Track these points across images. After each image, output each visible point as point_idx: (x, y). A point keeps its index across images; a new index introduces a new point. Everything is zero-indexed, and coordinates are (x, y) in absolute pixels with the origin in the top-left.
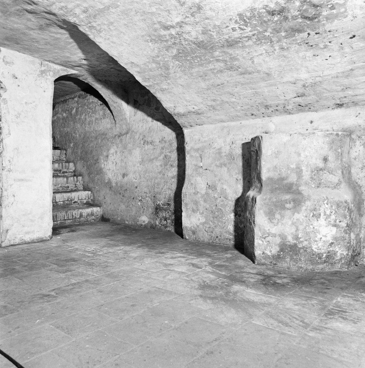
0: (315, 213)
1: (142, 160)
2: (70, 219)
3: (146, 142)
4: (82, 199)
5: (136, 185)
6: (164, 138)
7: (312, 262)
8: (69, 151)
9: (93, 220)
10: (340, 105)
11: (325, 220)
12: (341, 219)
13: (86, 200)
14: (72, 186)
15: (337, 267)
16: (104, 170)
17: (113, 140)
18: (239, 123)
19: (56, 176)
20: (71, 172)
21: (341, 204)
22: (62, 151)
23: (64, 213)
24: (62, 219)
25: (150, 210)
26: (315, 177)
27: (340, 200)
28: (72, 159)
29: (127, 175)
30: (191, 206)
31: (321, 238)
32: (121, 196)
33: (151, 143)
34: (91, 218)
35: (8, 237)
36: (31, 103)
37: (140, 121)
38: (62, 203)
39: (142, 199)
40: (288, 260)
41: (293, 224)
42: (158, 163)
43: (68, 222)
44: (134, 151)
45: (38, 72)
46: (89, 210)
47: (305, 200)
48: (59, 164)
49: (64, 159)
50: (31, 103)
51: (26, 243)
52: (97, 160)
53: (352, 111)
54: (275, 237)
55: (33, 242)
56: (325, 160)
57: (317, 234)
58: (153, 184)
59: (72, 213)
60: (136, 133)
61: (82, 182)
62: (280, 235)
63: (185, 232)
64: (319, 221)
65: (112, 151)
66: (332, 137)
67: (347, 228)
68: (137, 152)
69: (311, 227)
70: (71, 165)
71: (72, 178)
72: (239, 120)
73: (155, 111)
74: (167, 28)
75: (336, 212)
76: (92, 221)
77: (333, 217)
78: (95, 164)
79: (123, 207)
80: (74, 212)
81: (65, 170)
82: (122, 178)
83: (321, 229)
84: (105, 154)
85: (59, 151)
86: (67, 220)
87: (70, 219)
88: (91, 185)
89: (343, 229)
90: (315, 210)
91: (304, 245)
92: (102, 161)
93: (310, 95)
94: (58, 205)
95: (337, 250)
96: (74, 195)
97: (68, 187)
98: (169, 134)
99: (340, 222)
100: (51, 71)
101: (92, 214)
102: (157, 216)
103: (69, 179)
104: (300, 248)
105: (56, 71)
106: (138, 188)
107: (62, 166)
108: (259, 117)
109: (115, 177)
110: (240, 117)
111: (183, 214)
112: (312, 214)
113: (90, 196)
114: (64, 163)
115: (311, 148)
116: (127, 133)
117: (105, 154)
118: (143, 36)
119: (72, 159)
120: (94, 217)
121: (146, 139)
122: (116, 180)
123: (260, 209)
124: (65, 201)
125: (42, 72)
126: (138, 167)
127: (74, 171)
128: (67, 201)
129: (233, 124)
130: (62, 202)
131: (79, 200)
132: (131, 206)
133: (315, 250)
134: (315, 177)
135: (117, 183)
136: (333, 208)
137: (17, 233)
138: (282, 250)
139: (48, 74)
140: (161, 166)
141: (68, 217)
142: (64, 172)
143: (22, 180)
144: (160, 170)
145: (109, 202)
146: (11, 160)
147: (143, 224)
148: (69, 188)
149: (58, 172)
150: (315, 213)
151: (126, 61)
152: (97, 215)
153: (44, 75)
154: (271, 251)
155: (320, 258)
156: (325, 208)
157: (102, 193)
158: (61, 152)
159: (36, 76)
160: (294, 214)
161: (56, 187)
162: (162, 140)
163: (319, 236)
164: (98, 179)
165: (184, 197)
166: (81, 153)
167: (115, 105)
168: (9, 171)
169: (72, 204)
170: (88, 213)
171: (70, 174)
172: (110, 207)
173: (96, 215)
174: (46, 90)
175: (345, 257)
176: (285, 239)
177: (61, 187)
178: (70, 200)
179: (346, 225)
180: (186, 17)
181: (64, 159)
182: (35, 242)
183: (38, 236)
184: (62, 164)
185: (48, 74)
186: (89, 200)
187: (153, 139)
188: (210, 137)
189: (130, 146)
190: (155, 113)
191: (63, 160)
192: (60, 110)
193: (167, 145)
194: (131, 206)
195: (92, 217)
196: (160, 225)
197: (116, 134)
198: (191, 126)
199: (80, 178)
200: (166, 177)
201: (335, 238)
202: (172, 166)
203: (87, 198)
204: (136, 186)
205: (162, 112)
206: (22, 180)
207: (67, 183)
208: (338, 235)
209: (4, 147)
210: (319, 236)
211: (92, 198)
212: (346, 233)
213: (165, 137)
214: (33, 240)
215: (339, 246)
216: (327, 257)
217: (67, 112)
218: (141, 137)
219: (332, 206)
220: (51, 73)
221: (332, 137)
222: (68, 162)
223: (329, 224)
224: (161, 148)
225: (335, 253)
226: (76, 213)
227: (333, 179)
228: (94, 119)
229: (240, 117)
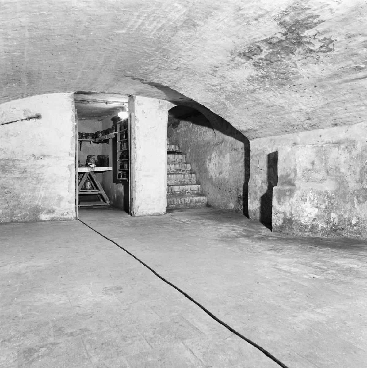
0: (303, 198)
1: (231, 162)
3: (233, 149)
5: (227, 181)
7: (301, 230)
8: (188, 155)
10: (336, 125)
11: (310, 203)
12: (321, 203)
15: (319, 235)
16: (208, 169)
17: (214, 147)
18: (280, 136)
19: (177, 173)
21: (321, 193)
23: (178, 199)
25: (235, 199)
26: (305, 175)
27: (321, 190)
28: (189, 162)
29: (222, 173)
30: (253, 195)
31: (307, 215)
32: (218, 189)
34: (198, 204)
35: (139, 211)
36: (153, 127)
38: (179, 192)
40: (287, 228)
41: (290, 205)
43: (181, 206)
44: (226, 155)
45: (158, 107)
46: (197, 198)
47: (296, 190)
48: (179, 164)
49: (185, 161)
50: (153, 127)
51: (149, 215)
52: (205, 162)
53: (344, 128)
54: (281, 214)
55: (153, 215)
56: (313, 163)
57: (305, 212)
62: (283, 212)
63: (249, 214)
64: (306, 204)
65: (213, 155)
66: (317, 148)
67: (326, 209)
68: (228, 156)
69: (300, 207)
70: (189, 165)
71: (188, 175)
72: (279, 135)
74: (214, 86)
75: (318, 198)
77: (316, 201)
78: (203, 165)
79: (219, 196)
80: (186, 199)
81: (184, 169)
82: (219, 175)
83: (307, 209)
84: (209, 157)
85: (181, 155)
88: (201, 180)
89: (323, 210)
90: (303, 196)
91: (295, 219)
92: (207, 163)
93: (313, 119)
94: (176, 194)
95: (319, 224)
96: (187, 187)
97: (185, 182)
98: (240, 145)
99: (321, 205)
101: (199, 201)
103: (185, 176)
104: (293, 221)
106: (228, 182)
107: (182, 166)
108: (291, 133)
110: (280, 133)
111: (249, 201)
112: (301, 199)
115: (302, 156)
116: (222, 142)
117: (209, 157)
118: (204, 90)
119: (189, 162)
120: (200, 203)
123: (274, 195)
125: (161, 107)
126: (228, 167)
127: (191, 170)
129: (277, 137)
131: (191, 191)
133: (303, 222)
134: (305, 175)
135: (216, 179)
136: (316, 195)
137: (144, 209)
138: (284, 222)
139: (164, 107)
142: (183, 171)
143: (148, 176)
145: (211, 193)
146: (141, 164)
148: (186, 182)
149: (178, 171)
150: (303, 198)
151: (201, 102)
152: (203, 202)
154: (279, 223)
155: (306, 228)
156: (310, 195)
157: (207, 187)
160: (290, 199)
161: (176, 181)
163: (306, 214)
164: (205, 176)
165: (249, 189)
166: (195, 156)
168: (140, 170)
169: (186, 194)
172: (211, 196)
174: (163, 118)
175: (324, 229)
176: (286, 215)
179: (325, 207)
180: (220, 81)
181: (185, 161)
182: (155, 215)
184: (182, 165)
185: (164, 107)
186: (199, 191)
187: (237, 146)
188: (264, 146)
192: (183, 125)
199: (194, 175)
201: (317, 216)
206: (148, 176)
207: (184, 178)
208: (319, 214)
209: (137, 156)
210: (306, 214)
211: (201, 190)
212: (325, 213)
214: (154, 214)
215: (320, 221)
216: (311, 228)
217: (187, 127)
218: (230, 146)
219: (315, 194)
220: (166, 107)
221: (317, 148)
222: (187, 163)
223: (313, 206)
225: (317, 226)
226: (188, 200)
227: (318, 176)
228: (202, 132)
229: (280, 133)
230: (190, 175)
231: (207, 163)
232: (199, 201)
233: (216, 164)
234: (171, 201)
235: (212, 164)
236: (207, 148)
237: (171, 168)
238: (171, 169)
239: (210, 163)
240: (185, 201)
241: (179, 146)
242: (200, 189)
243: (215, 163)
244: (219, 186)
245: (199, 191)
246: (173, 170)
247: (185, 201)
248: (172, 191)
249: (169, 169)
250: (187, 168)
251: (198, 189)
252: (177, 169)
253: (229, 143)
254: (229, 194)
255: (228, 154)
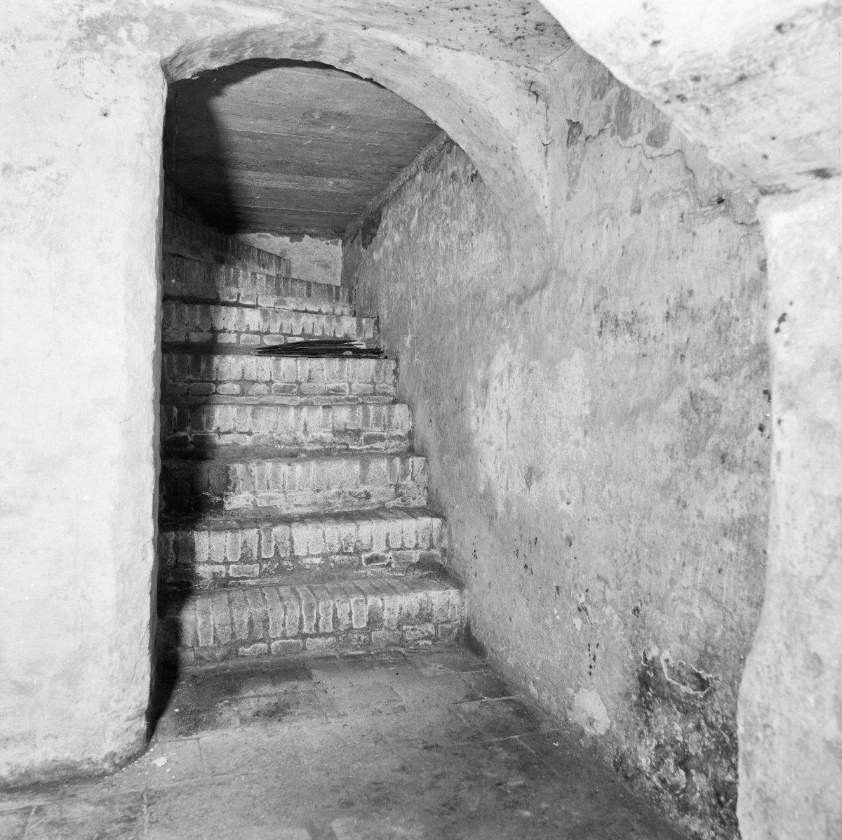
1: (594, 414)
2: (325, 635)
3: (610, 324)
4: (402, 548)
5: (567, 531)
6: (691, 293)
9: (428, 638)
13: (419, 552)
14: (383, 494)
16: (476, 442)
19: (340, 450)
20: (400, 437)
22: (385, 362)
24: (288, 634)
25: (618, 674)
29: (539, 478)
33: (628, 324)
37: (588, 217)
38: (317, 561)
39: (589, 608)
42: (660, 437)
44: (564, 366)
45: (71, 30)
46: (410, 601)
49: (391, 390)
58: (631, 541)
59: (335, 611)
60: (573, 280)
61: (425, 478)
65: (499, 365)
68: (574, 370)
70: (400, 411)
71: (384, 464)
73: (649, 149)
76: (421, 643)
78: (455, 414)
81: (376, 431)
82: (524, 486)
84: (480, 374)
86: (313, 636)
87: (325, 635)
92: (473, 404)
94: (302, 568)
97: (368, 496)
100: (136, 20)
101: (424, 616)
102: (647, 723)
103: (372, 466)
105: (167, 19)
106: (575, 544)
107: (366, 416)
109: (505, 477)
113: (435, 536)
114: (371, 408)
116: (543, 284)
119: (407, 395)
121: (608, 305)
122: (507, 489)
124: (332, 553)
126: (577, 443)
127: (410, 435)
128: (338, 554)
130: (318, 556)
131: (389, 549)
132: (549, 621)
140: (670, 449)
141: (317, 626)
142: (369, 440)
144: (666, 473)
147: (587, 729)
148: (373, 500)
149: (347, 439)
152: (448, 622)
153: (101, 39)
158: (379, 366)
159: (62, 45)
161: (319, 495)
162: (681, 307)
167: (493, 163)
169: (360, 566)
170: (404, 611)
171: (394, 443)
173: (442, 619)
174: (112, 109)
177: (339, 494)
178: (351, 550)
181: (391, 390)
183: (51, 756)
185: (123, 33)
186: (434, 552)
189: (552, 339)
190: (648, 165)
191: (384, 394)
192: (390, 224)
193: (700, 334)
194: (549, 621)
195: (423, 628)
196: (655, 779)
197: (510, 290)
198: (822, 174)
199: (416, 462)
200: (694, 519)
202: (723, 459)
203: (426, 545)
204: (569, 532)
205: (680, 152)
207: (364, 481)
213: (695, 287)
214: (28, 774)
218: (591, 299)
220: (141, 30)
224: (671, 352)
230: (397, 461)
231: (473, 404)
232: (419, 615)
233: (509, 419)
234: (251, 623)
235: (494, 416)
236: (473, 320)
237: (305, 425)
238: (306, 432)
239: (484, 405)
240: (335, 618)
241: (377, 322)
242: (440, 539)
243: (508, 411)
244: (524, 549)
245: (434, 552)
246: (317, 435)
247: (335, 618)
248: (277, 553)
249: (295, 432)
250: (390, 422)
251: (431, 541)
252: (339, 432)
253: (580, 284)
254: (578, 622)
255: (578, 355)
